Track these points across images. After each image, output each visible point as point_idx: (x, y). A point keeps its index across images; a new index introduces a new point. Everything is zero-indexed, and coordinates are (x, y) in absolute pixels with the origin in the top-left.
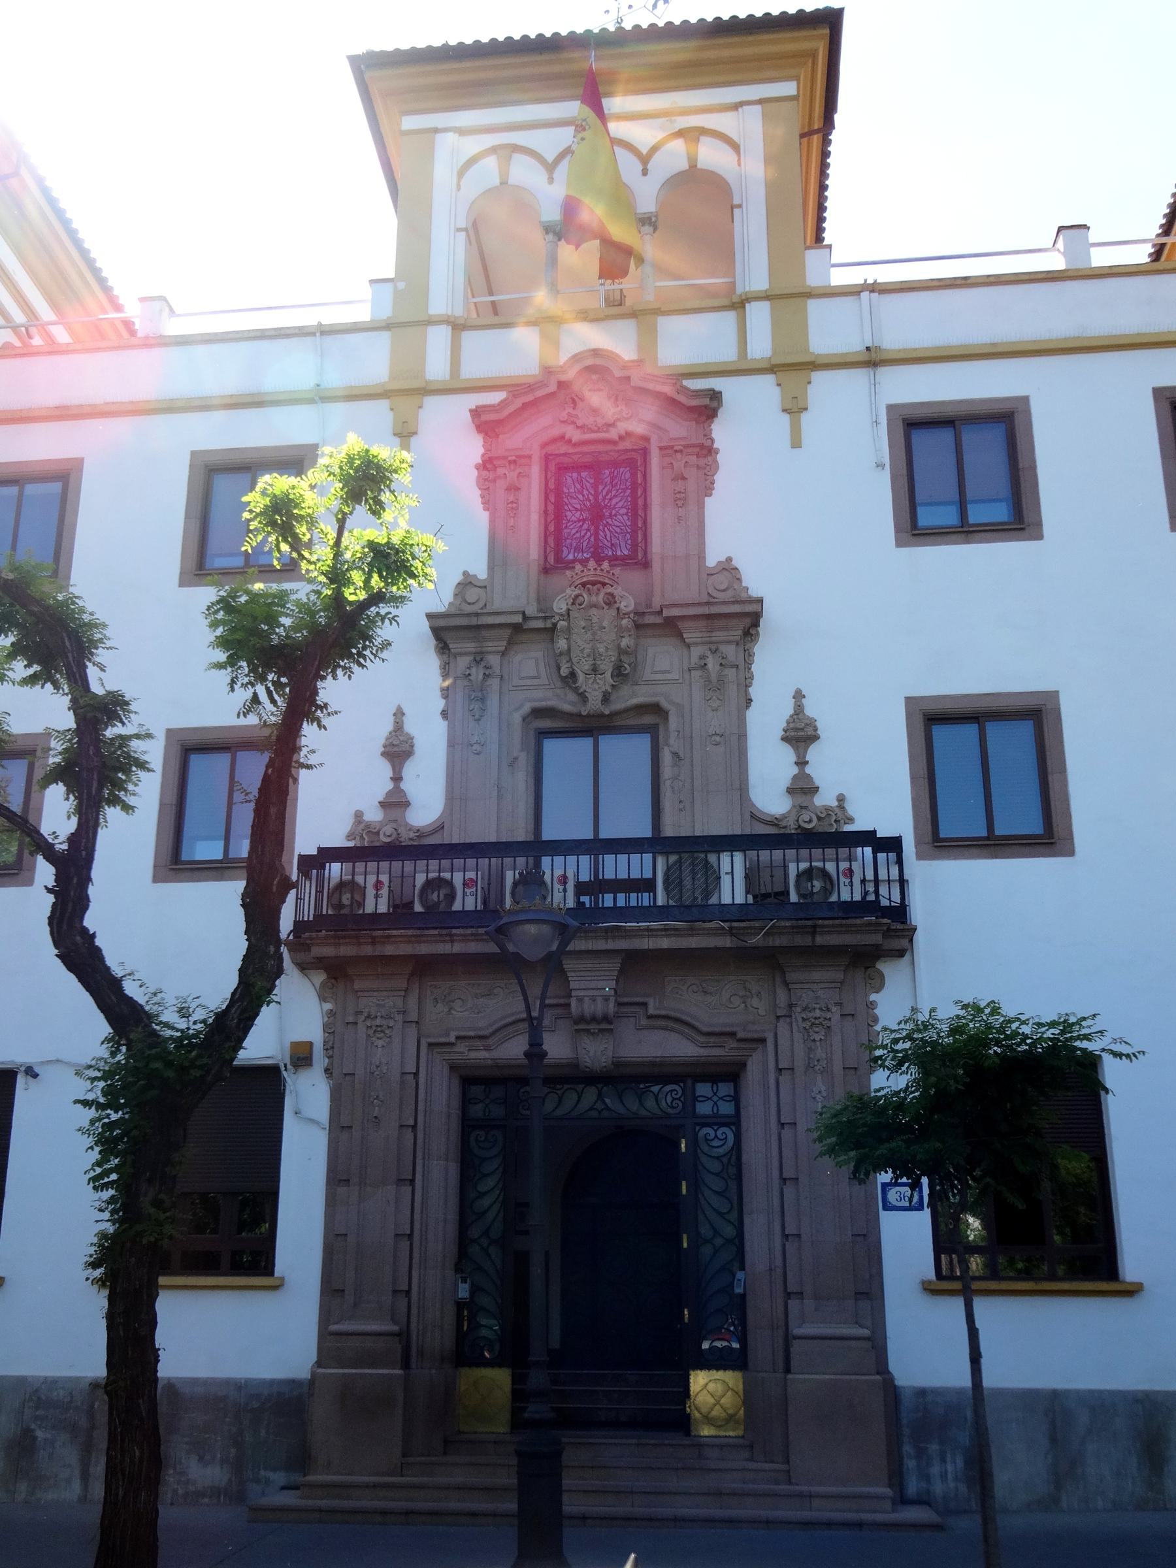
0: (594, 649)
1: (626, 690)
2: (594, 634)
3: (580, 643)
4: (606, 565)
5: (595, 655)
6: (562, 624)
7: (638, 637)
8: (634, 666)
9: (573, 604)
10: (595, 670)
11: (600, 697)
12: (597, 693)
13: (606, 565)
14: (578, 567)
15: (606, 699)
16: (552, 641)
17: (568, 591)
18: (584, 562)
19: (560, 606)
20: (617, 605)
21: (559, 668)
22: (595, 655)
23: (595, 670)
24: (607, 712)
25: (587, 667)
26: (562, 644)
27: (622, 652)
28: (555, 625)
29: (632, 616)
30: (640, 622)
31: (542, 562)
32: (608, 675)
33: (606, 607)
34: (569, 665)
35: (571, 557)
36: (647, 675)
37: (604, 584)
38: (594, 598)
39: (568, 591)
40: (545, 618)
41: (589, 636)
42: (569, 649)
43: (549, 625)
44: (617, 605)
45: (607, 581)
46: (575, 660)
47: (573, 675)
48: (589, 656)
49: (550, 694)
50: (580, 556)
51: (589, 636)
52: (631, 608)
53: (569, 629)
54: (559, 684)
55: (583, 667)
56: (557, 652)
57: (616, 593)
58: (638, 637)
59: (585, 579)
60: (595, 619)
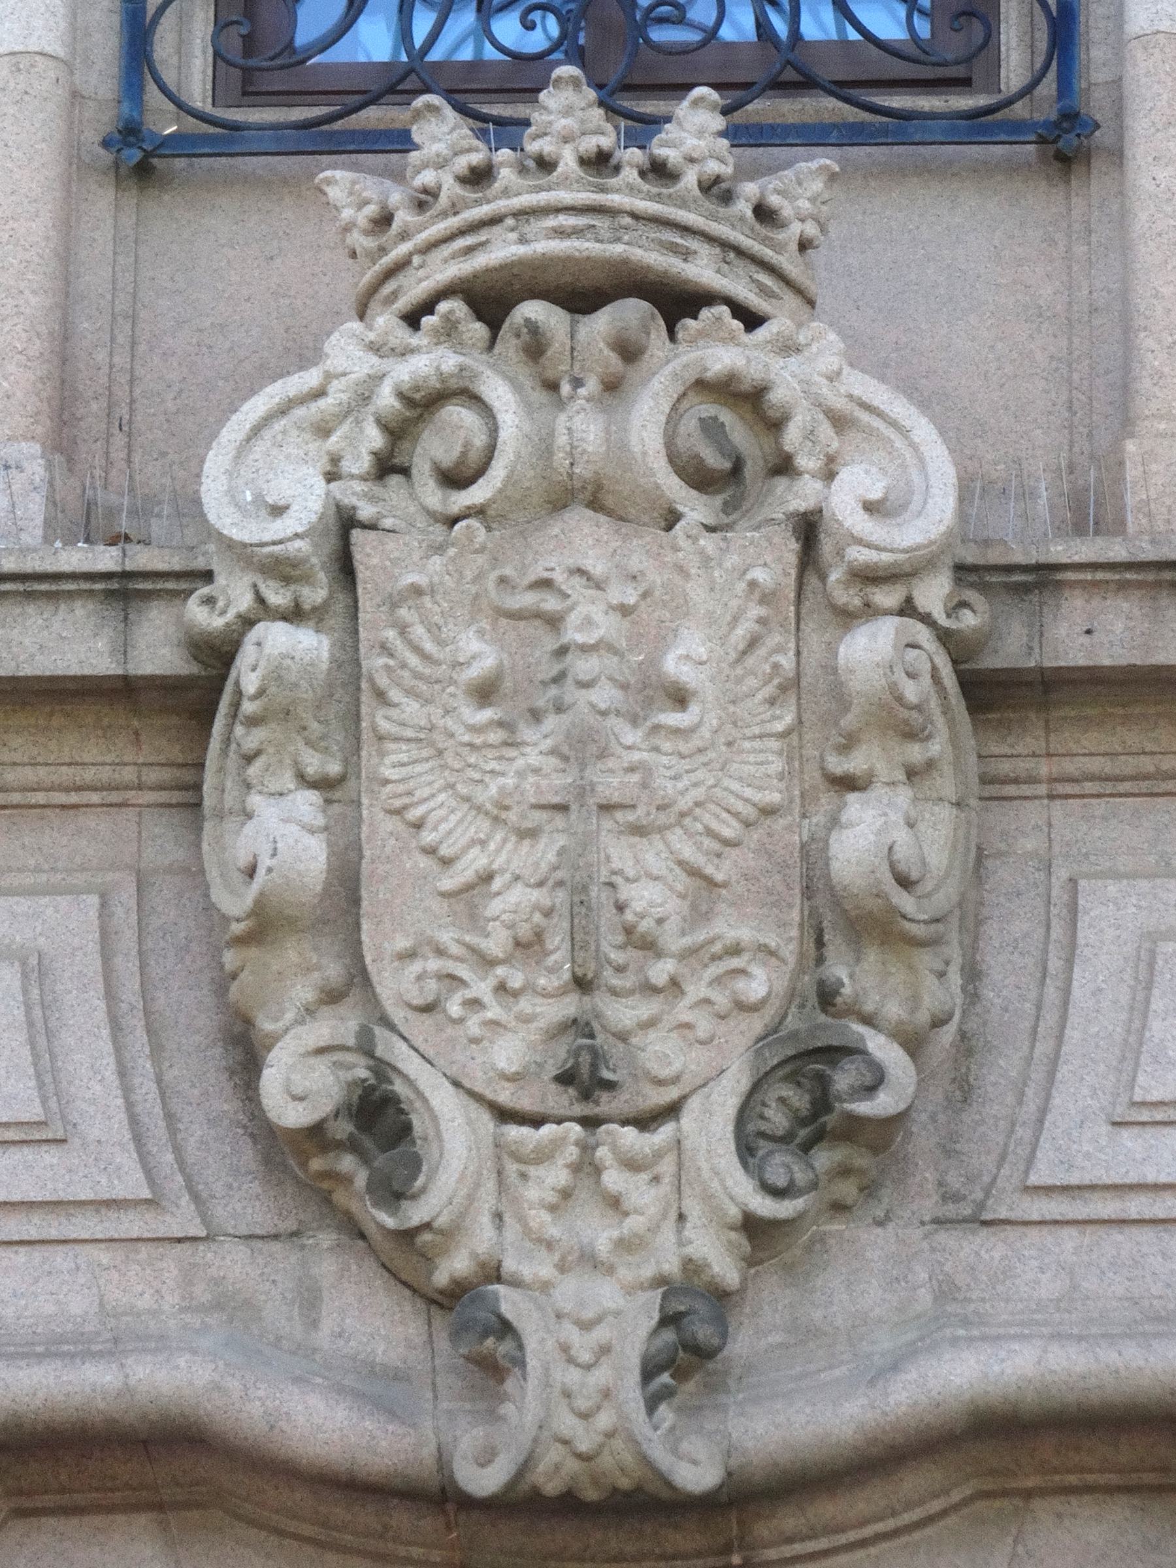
0: (580, 892)
1: (871, 1272)
2: (583, 748)
3: (450, 826)
4: (694, 129)
5: (589, 944)
6: (284, 649)
7: (994, 787)
8: (955, 1052)
9: (388, 467)
10: (586, 1078)
11: (635, 1328)
12: (606, 1294)
13: (694, 129)
14: (441, 136)
15: (688, 1348)
16: (188, 801)
17: (347, 353)
18: (494, 96)
19: (264, 482)
20: (802, 494)
21: (245, 1053)
22: (589, 944)
23: (586, 1078)
24: (697, 1473)
25: (508, 1053)
26: (278, 833)
27: (844, 920)
28: (217, 654)
29: (933, 594)
30: (1012, 650)
31: (102, 77)
32: (709, 1126)
33: (697, 509)
34: (337, 1026)
35: (374, 41)
36: (1080, 1142)
37: (678, 303)
38: (583, 428)
39: (347, 353)
40: (123, 592)
41: (532, 765)
42: (346, 886)
43: (156, 650)
44: (802, 494)
45: (703, 270)
46: (395, 985)
47: (378, 1117)
48: (528, 946)
49: (147, 1288)
50: (458, 40)
51: (532, 765)
52: (931, 520)
53: (349, 688)
54: (246, 1203)
55: (467, 1062)
56: (235, 903)
57: (786, 382)
58: (994, 787)
59: (503, 249)
60: (590, 619)
